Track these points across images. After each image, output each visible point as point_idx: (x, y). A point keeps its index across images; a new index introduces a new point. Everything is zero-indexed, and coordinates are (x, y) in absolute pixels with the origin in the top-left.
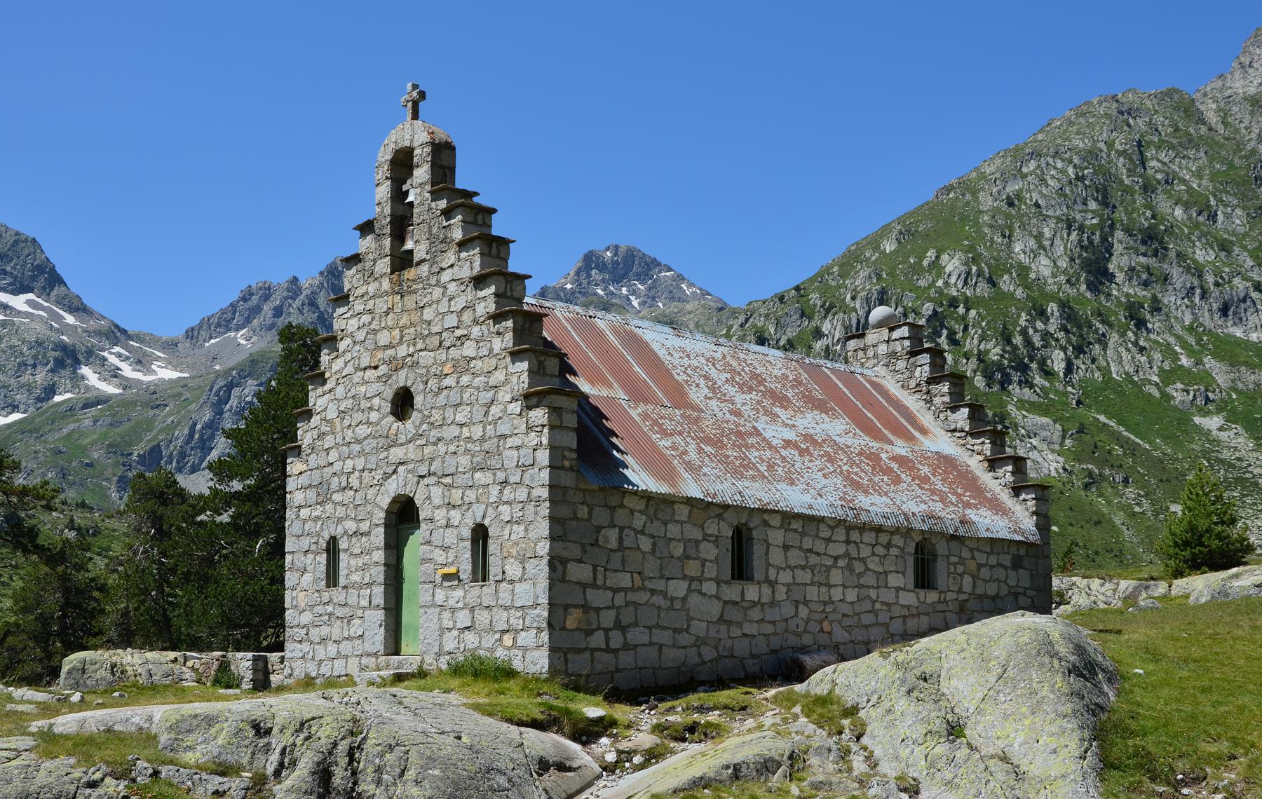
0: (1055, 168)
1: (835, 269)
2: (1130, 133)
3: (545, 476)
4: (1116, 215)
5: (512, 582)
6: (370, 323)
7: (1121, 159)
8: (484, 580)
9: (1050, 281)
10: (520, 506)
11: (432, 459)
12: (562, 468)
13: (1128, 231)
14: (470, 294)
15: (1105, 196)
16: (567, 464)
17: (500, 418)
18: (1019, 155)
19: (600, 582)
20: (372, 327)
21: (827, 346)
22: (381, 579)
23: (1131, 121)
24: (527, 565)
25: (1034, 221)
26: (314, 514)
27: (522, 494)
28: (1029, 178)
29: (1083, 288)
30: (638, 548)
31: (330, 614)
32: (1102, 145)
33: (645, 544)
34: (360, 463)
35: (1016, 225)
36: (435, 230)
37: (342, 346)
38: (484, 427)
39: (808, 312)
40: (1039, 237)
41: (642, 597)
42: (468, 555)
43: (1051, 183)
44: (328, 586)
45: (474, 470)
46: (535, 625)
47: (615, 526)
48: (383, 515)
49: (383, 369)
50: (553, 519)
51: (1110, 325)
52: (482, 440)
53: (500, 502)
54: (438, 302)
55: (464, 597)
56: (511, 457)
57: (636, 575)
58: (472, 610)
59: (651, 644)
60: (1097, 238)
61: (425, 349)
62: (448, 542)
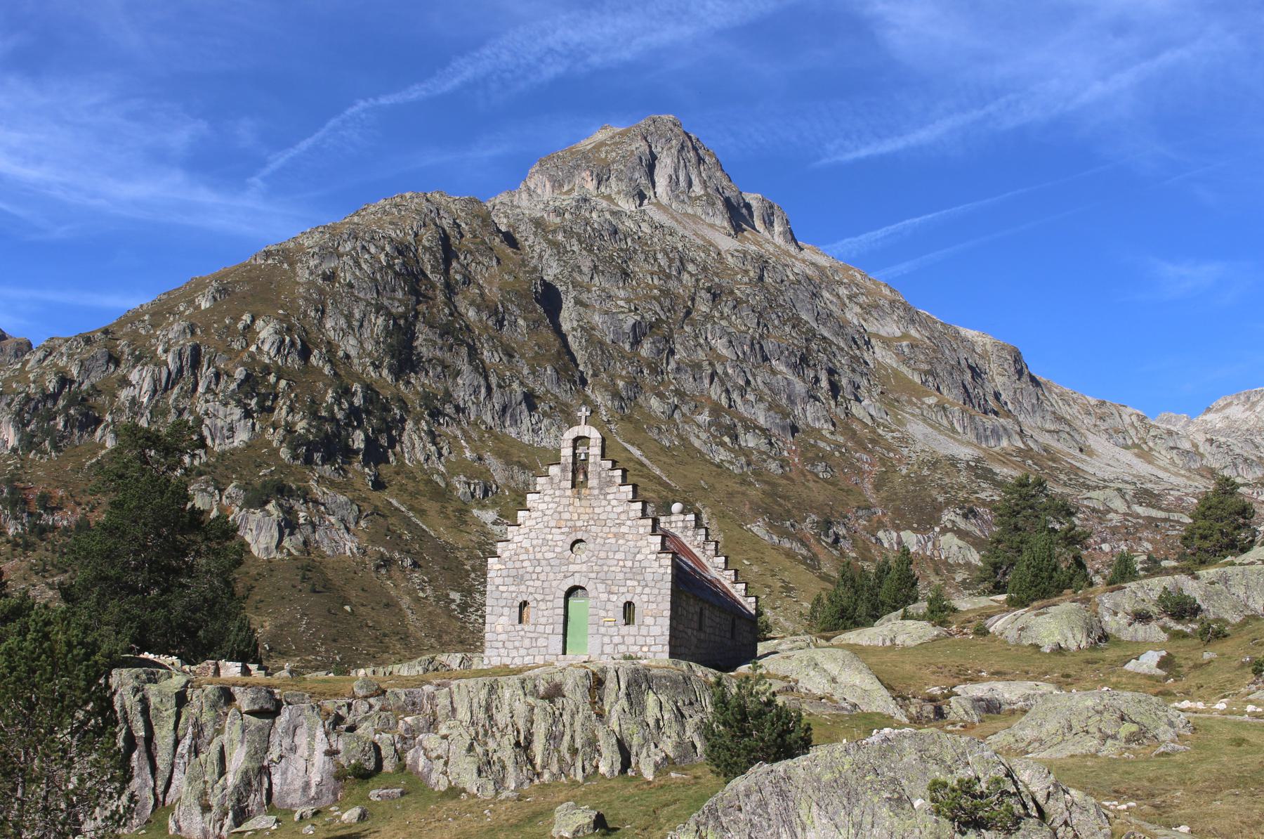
21: (134, 397)
27: (656, 591)
35: (329, 302)
40: (349, 317)
43: (364, 266)
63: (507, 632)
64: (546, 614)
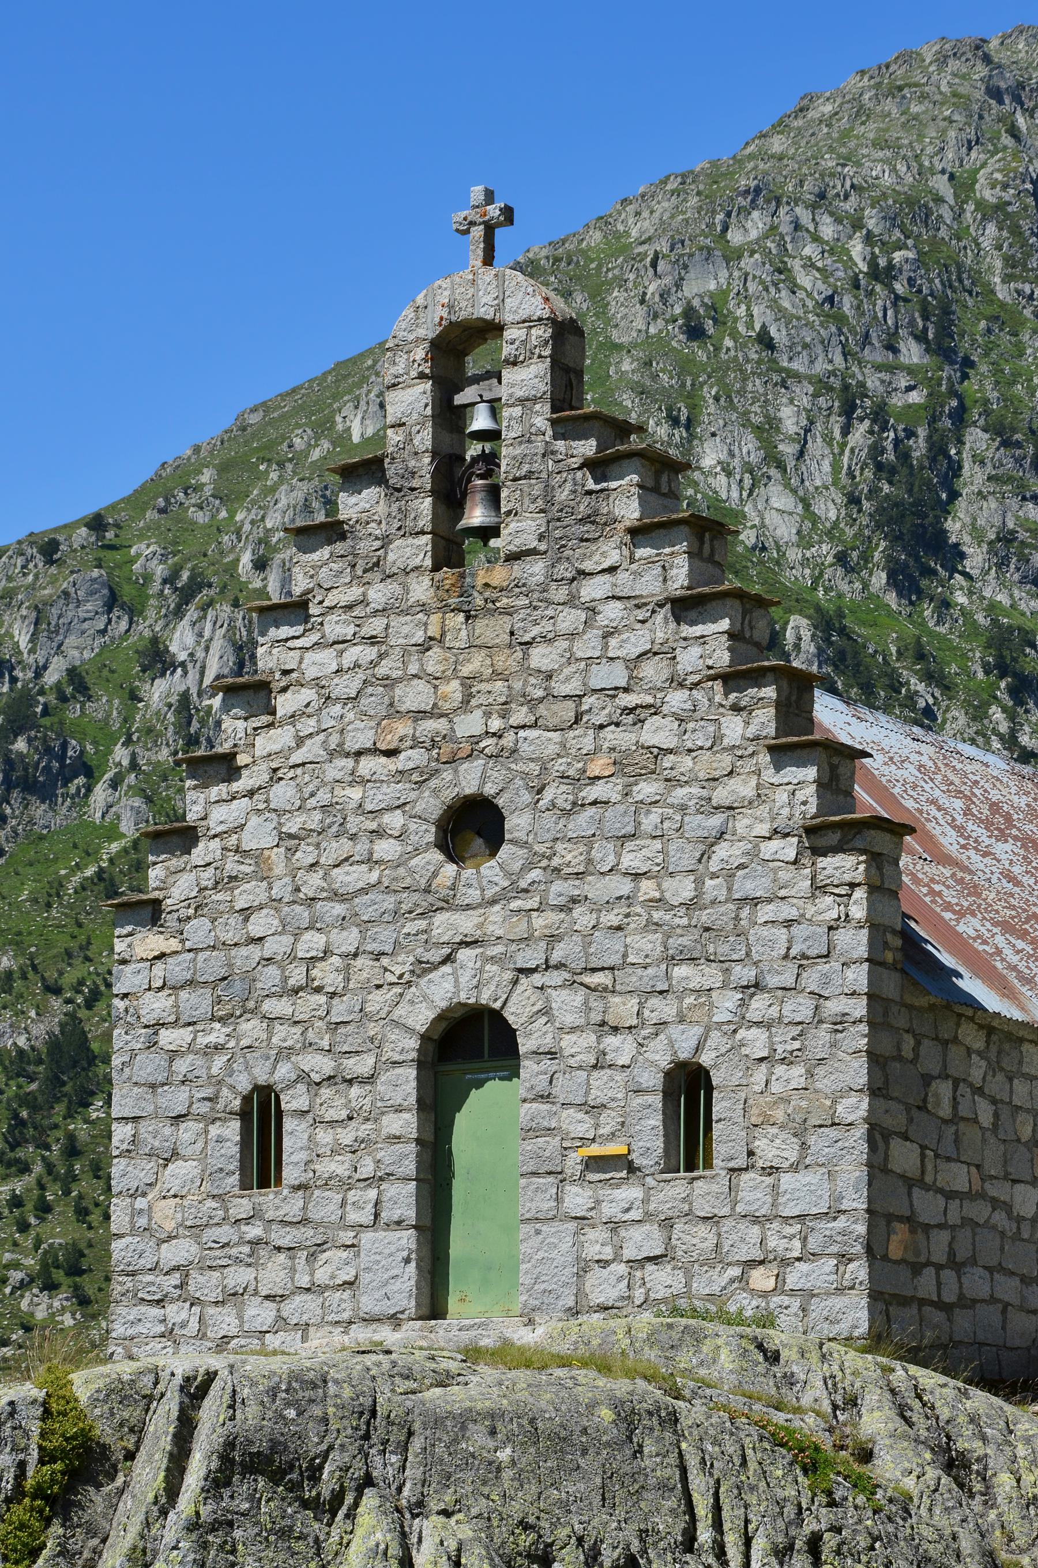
0: (816, 239)
1: (207, 476)
2: (1015, 156)
3: (859, 977)
4: (971, 386)
5: (771, 1170)
6: (373, 664)
7: (991, 229)
8: (691, 1167)
9: (794, 555)
10: (796, 1031)
11: (553, 939)
12: (882, 964)
13: (1002, 433)
14: (662, 627)
15: (945, 330)
16: (889, 956)
17: (741, 867)
18: (731, 193)
19: (929, 1179)
20: (381, 671)
21: (185, 696)
22: (410, 1167)
23: (1021, 121)
24: (812, 1140)
25: (756, 385)
26: (203, 1040)
27: (800, 1008)
28: (747, 263)
29: (879, 579)
30: (976, 1121)
31: (255, 1243)
32: (941, 185)
33: (985, 1114)
34: (348, 940)
35: (709, 392)
36: (563, 495)
37: (285, 704)
38: (699, 883)
39: (127, 592)
40: (767, 431)
41: (980, 1211)
42: (656, 1120)
43: (804, 280)
44: (245, 1185)
45: (672, 960)
46: (834, 1249)
47: (947, 1077)
48: (414, 1043)
49: (412, 758)
50: (875, 1058)
51: (947, 688)
52: (691, 906)
53: (741, 1021)
54: (572, 635)
55: (646, 1201)
56: (769, 941)
57: (973, 1170)
58: (667, 1224)
59: (993, 1300)
60: (919, 447)
61: (535, 725)
62: (597, 1095)
63: (196, 1229)
64: (355, 1135)
